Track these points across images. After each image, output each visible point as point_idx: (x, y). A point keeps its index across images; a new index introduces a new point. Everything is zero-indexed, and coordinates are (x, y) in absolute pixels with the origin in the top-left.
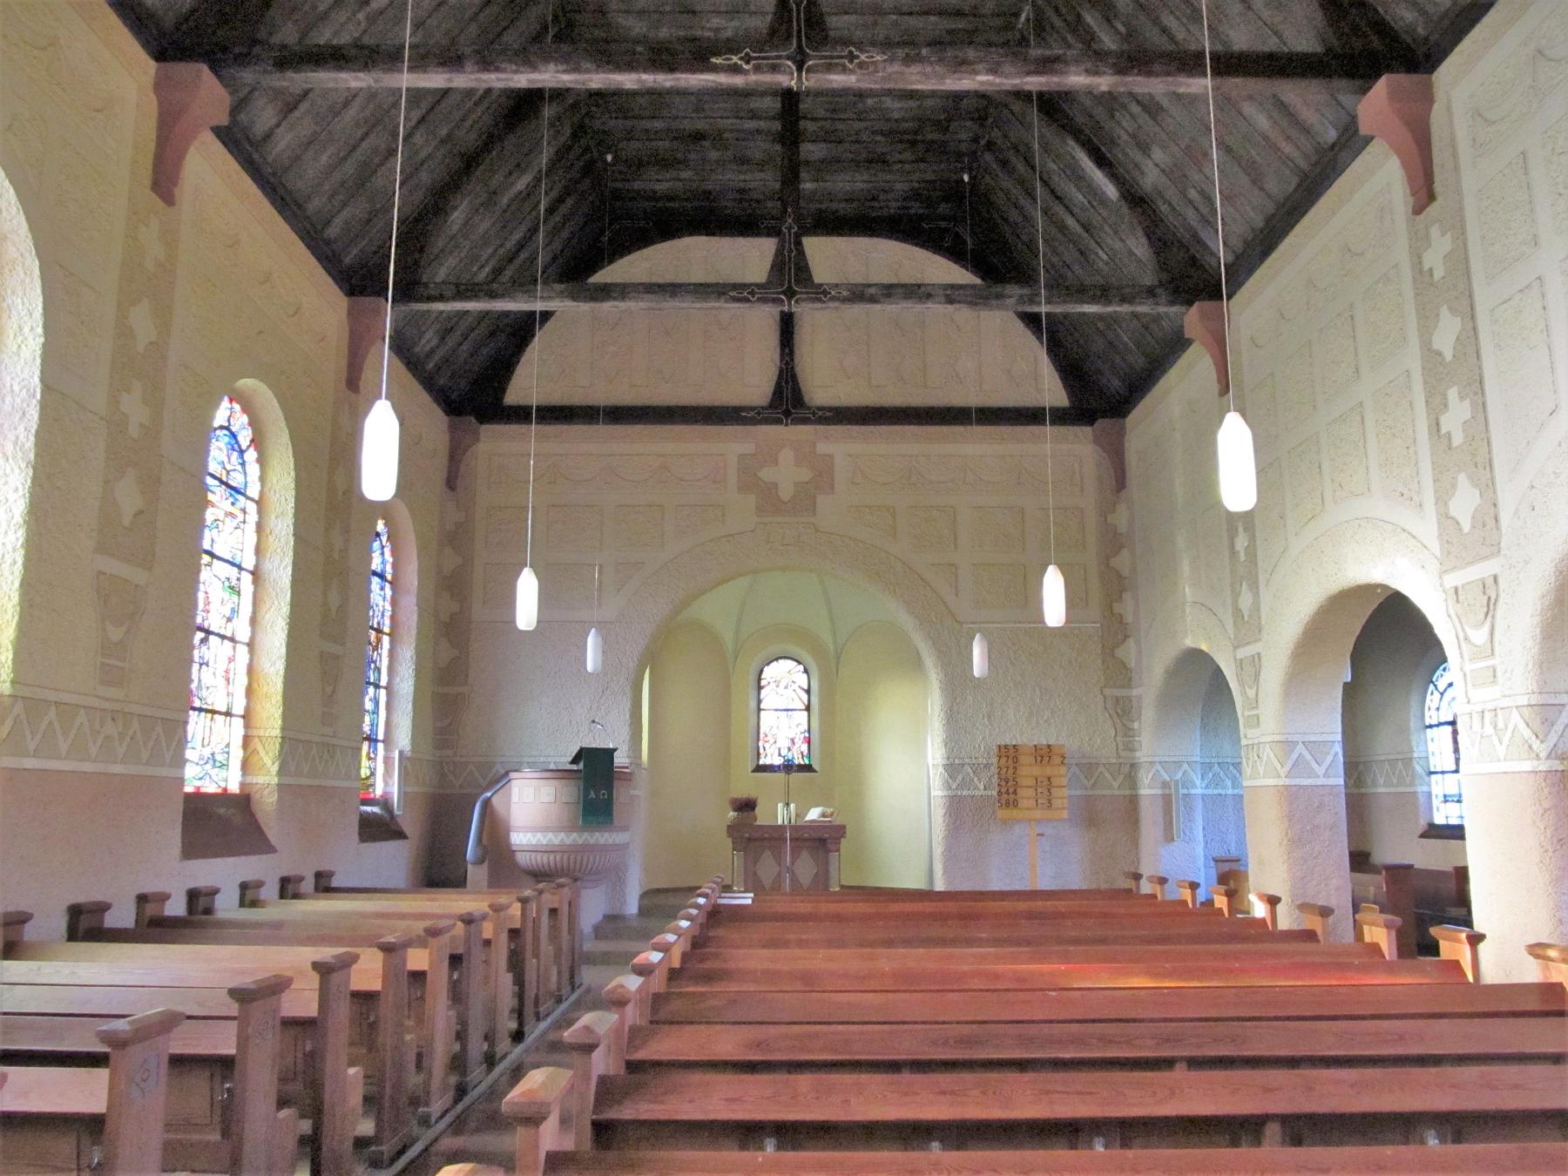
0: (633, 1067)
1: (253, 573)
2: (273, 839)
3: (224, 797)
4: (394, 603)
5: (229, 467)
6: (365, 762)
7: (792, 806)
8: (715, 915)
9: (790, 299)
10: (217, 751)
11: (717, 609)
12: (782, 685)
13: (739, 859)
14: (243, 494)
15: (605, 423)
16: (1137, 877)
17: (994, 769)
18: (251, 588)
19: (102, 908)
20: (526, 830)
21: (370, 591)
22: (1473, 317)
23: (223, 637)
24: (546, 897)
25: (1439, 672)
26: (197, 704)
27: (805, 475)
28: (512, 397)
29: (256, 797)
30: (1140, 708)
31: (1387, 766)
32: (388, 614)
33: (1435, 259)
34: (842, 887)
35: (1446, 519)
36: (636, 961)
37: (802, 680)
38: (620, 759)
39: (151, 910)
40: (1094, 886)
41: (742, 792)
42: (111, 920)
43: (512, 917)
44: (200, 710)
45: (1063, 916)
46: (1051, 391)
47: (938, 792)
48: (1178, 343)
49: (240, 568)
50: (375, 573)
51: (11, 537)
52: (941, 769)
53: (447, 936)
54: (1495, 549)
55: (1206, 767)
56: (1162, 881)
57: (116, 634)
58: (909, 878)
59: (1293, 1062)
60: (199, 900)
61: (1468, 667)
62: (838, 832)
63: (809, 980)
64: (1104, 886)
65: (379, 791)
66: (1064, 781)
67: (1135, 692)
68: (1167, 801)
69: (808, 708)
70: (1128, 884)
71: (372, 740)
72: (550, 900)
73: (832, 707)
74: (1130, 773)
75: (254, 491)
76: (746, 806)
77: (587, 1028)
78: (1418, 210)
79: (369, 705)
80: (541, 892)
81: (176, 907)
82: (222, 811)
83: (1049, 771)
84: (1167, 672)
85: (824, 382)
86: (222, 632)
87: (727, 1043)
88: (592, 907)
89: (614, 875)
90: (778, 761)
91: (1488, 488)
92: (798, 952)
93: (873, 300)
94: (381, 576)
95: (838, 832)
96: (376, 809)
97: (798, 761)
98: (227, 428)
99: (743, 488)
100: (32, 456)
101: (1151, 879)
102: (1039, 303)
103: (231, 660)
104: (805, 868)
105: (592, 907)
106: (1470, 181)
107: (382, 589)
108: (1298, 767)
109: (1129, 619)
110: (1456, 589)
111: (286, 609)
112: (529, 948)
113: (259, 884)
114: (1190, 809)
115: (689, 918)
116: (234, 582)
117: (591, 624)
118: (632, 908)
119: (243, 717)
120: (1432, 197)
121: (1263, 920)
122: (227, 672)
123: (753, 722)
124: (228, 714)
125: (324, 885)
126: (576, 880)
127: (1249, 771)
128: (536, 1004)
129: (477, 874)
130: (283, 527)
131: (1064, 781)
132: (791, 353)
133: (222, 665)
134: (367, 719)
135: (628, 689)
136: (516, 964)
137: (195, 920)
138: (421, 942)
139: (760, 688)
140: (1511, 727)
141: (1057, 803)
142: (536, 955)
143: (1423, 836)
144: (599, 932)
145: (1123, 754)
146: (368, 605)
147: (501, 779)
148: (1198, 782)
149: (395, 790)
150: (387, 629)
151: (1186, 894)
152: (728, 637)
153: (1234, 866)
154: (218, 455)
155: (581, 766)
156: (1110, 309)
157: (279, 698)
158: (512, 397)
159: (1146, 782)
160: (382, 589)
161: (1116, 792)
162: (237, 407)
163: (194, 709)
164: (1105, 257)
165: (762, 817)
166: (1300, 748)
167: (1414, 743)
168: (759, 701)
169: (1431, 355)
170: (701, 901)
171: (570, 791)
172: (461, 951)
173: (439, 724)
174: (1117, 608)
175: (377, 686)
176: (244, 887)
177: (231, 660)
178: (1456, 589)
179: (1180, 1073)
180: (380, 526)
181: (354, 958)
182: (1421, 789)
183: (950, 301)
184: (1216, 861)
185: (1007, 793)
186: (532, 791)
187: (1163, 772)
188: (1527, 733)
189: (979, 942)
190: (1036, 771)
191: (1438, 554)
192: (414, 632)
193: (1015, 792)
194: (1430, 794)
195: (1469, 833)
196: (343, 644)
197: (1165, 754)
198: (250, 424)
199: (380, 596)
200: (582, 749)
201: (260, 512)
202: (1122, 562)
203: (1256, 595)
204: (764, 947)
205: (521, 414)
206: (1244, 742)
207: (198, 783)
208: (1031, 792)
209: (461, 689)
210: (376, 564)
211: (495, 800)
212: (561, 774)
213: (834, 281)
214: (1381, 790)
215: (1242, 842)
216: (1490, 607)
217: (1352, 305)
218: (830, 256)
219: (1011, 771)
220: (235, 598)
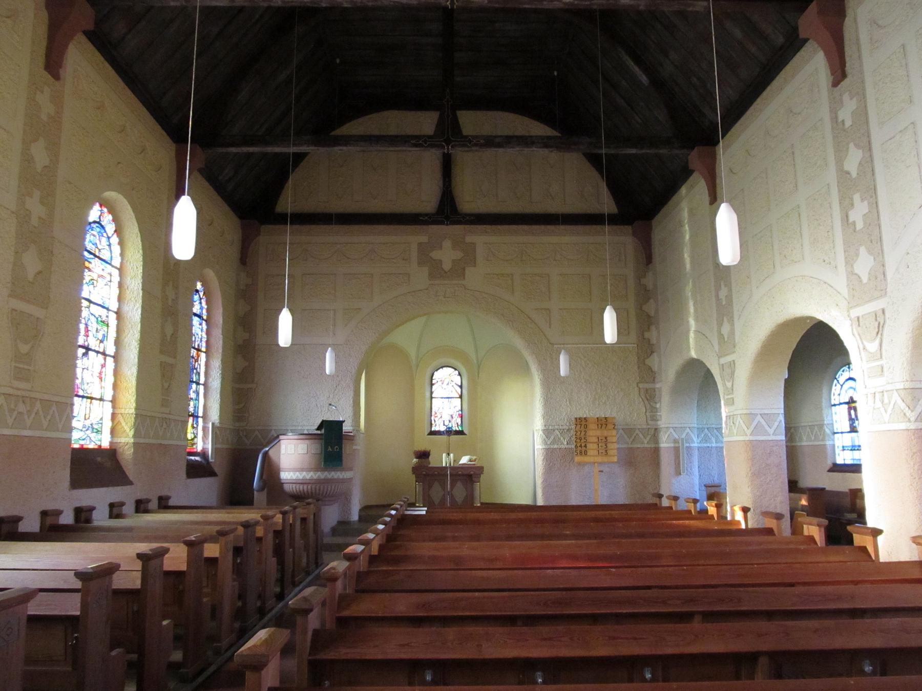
0: (343, 622)
1: (116, 313)
2: (131, 477)
3: (99, 450)
4: (208, 333)
6: (190, 430)
7: (452, 455)
8: (403, 521)
9: (448, 145)
10: (94, 422)
11: (406, 336)
12: (446, 383)
13: (419, 487)
14: (110, 264)
15: (336, 224)
16: (660, 496)
17: (573, 433)
18: (115, 322)
19: (17, 520)
20: (289, 470)
21: (192, 326)
22: (870, 149)
23: (98, 352)
24: (300, 511)
25: (840, 372)
26: (81, 393)
28: (279, 209)
29: (120, 451)
30: (661, 395)
31: (808, 429)
32: (204, 340)
33: (846, 115)
34: (482, 504)
35: (852, 275)
36: (346, 551)
37: (458, 380)
38: (347, 427)
39: (49, 521)
40: (632, 502)
41: (421, 447)
42: (23, 527)
43: (276, 523)
44: (83, 397)
45: (616, 520)
46: (607, 204)
47: (539, 446)
48: (685, 173)
49: (108, 309)
50: (195, 315)
52: (541, 432)
53: (232, 535)
54: (883, 293)
55: (700, 430)
56: (676, 498)
57: (24, 348)
58: (521, 497)
59: (770, 615)
60: (83, 515)
62: (480, 469)
63: (458, 563)
64: (640, 502)
65: (199, 448)
67: (658, 386)
68: (677, 450)
69: (461, 397)
70: (655, 500)
71: (195, 416)
72: (300, 511)
73: (475, 396)
75: (117, 262)
76: (423, 455)
77: (305, 599)
78: (835, 84)
79: (193, 395)
80: (295, 508)
81: (67, 518)
82: (99, 459)
83: (605, 433)
85: (470, 199)
86: (97, 349)
87: (402, 605)
88: (330, 516)
89: (344, 498)
90: (443, 429)
91: (879, 254)
92: (452, 544)
93: (499, 145)
94: (199, 316)
95: (480, 469)
96: (197, 458)
97: (455, 428)
98: (98, 223)
99: (421, 263)
101: (669, 497)
102: (601, 148)
103: (103, 366)
104: (459, 492)
105: (330, 516)
107: (201, 324)
108: (758, 429)
109: (654, 341)
110: (858, 318)
112: (287, 543)
113: (122, 504)
114: (690, 455)
115: (385, 523)
116: (104, 318)
117: (329, 345)
118: (355, 517)
119: (111, 401)
120: (844, 75)
122: (100, 373)
123: (428, 405)
124: (101, 399)
125: (164, 504)
126: (318, 500)
128: (293, 576)
129: (259, 497)
130: (135, 284)
131: (615, 439)
132: (450, 181)
133: (98, 368)
134: (192, 403)
136: (279, 551)
137: (81, 526)
138: (212, 539)
139: (432, 385)
140: (892, 403)
141: (610, 452)
142: (292, 546)
143: (830, 471)
144: (334, 531)
145: (650, 422)
146: (191, 334)
147: (274, 439)
148: (695, 439)
149: (209, 447)
150: (204, 349)
151: (691, 506)
152: (413, 353)
154: (91, 239)
155: (323, 431)
156: (644, 151)
157: (134, 389)
158: (279, 209)
159: (664, 439)
160: (201, 324)
161: (646, 446)
162: (105, 210)
163: (79, 396)
164: (639, 121)
165: (433, 462)
168: (432, 393)
169: (843, 174)
170: (393, 512)
171: (316, 447)
172: (241, 544)
173: (237, 407)
174: (646, 335)
175: (198, 384)
176: (112, 506)
177: (103, 366)
178: (858, 318)
179: (697, 624)
180: (199, 286)
181: (167, 550)
182: (828, 443)
183: (546, 146)
184: (706, 486)
185: (581, 446)
186: (293, 446)
187: (674, 433)
188: (903, 406)
189: (566, 537)
190: (598, 433)
191: (846, 297)
192: (221, 351)
193: (585, 446)
194: (834, 446)
195: (864, 469)
196: (175, 358)
197: (676, 423)
198: (113, 220)
199: (198, 329)
200: (323, 422)
201: (121, 275)
202: (650, 308)
203: (732, 325)
204: (431, 541)
205: (281, 219)
207: (82, 442)
208: (595, 446)
209: (250, 386)
210: (196, 309)
211: (271, 453)
212: (310, 436)
213: (474, 134)
214: (804, 444)
215: (722, 473)
216: (880, 329)
218: (472, 122)
219: (583, 433)
220: (105, 328)
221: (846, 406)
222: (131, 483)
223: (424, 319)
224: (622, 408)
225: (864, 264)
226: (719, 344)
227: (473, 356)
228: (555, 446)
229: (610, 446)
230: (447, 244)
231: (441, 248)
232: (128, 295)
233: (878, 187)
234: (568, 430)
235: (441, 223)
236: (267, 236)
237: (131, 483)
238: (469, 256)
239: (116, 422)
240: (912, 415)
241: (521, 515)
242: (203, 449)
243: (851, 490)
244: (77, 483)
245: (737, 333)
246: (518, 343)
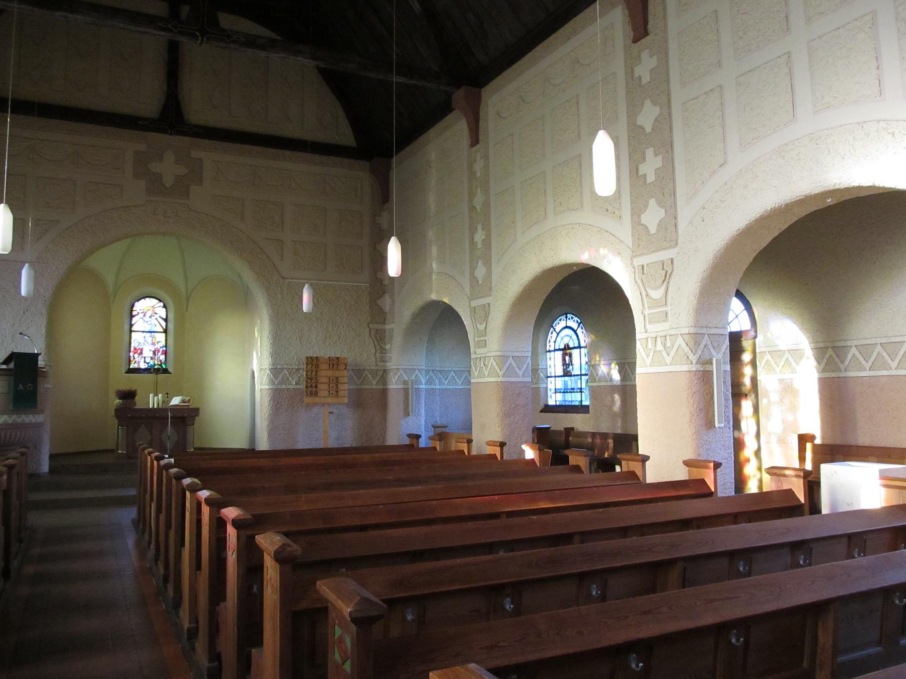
11: (104, 262)
13: (122, 431)
27: (182, 170)
34: (195, 449)
35: (638, 225)
37: (162, 312)
38: (41, 363)
41: (125, 387)
46: (345, 136)
48: (443, 109)
52: (268, 372)
61: (647, 312)
62: (195, 412)
66: (346, 380)
67: (388, 327)
69: (165, 331)
73: (179, 328)
74: (383, 375)
76: (128, 396)
83: (337, 374)
84: (413, 314)
85: (198, 111)
90: (143, 366)
95: (195, 412)
106: (673, 26)
108: (509, 371)
110: (643, 267)
118: (45, 468)
121: (533, 460)
123: (127, 338)
127: (476, 374)
135: (44, 311)
139: (132, 316)
141: (341, 393)
152: (110, 279)
153: (444, 430)
155: (12, 365)
156: (412, 82)
159: (394, 381)
161: (374, 387)
165: (139, 403)
166: (510, 360)
167: (540, 361)
168: (131, 325)
178: (643, 267)
185: (311, 386)
188: (687, 349)
190: (330, 373)
193: (316, 387)
206: (473, 356)
217: (577, 96)
219: (314, 373)
221: (560, 353)
223: (124, 243)
224: (352, 348)
225: (653, 216)
226: (471, 286)
229: (341, 387)
230: (170, 156)
233: (675, 144)
234: (297, 370)
240: (694, 358)
241: (309, 460)
243: (565, 429)
245: (494, 278)
246: (248, 276)
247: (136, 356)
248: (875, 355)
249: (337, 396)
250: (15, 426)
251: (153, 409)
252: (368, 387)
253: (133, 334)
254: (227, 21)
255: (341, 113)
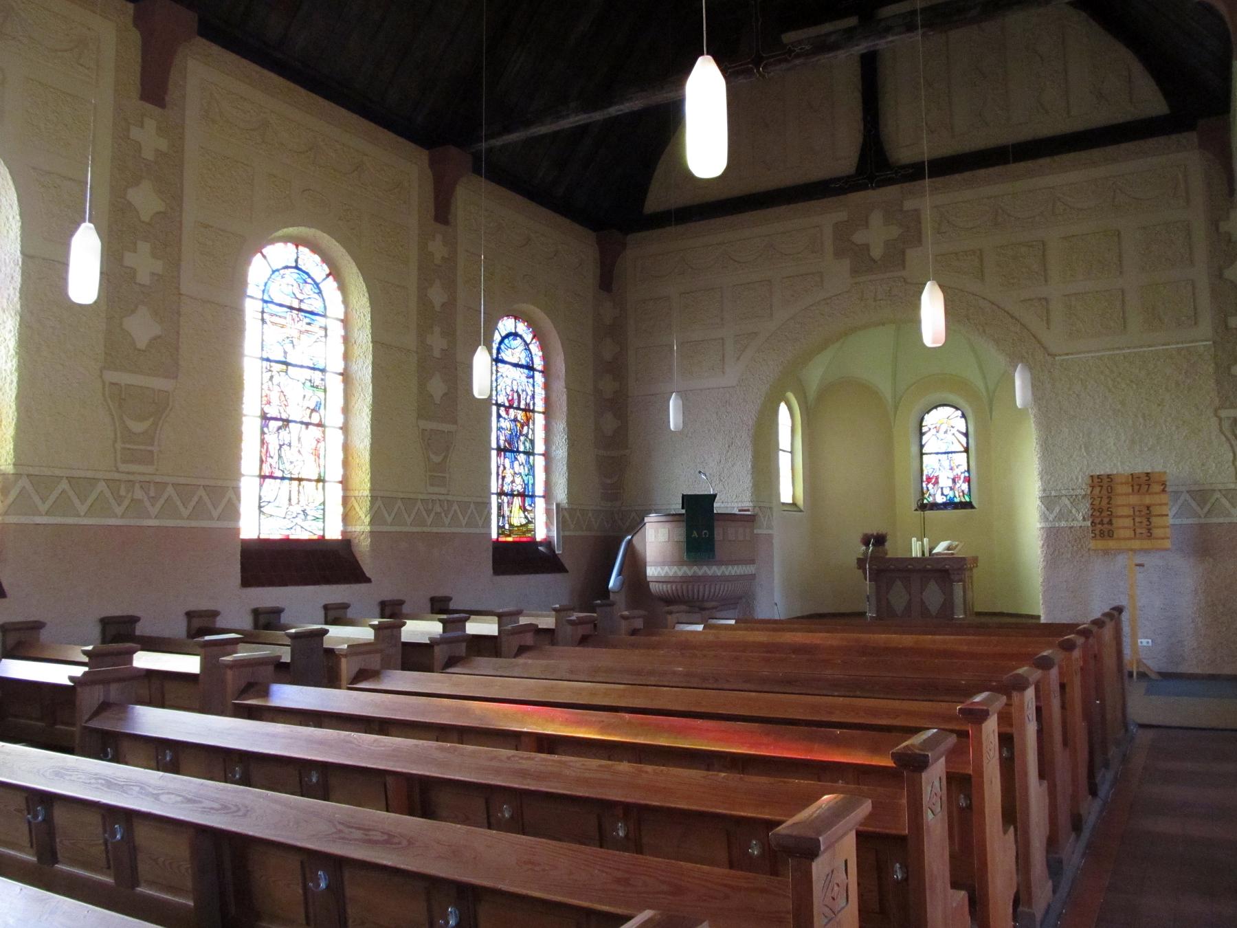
2: (368, 570)
5: (301, 297)
12: (942, 431)
13: (867, 586)
27: (895, 231)
37: (961, 425)
51: (9, 364)
65: (540, 535)
69: (967, 450)
83: (1148, 500)
90: (940, 499)
99: (839, 254)
100: (18, 306)
111: (369, 399)
135: (748, 443)
139: (922, 434)
141: (1157, 532)
147: (637, 525)
150: (540, 406)
152: (886, 389)
168: (922, 446)
171: (680, 532)
190: (1134, 500)
192: (565, 409)
193: (1110, 523)
196: (455, 422)
211: (635, 541)
212: (673, 518)
219: (1105, 502)
222: (368, 580)
227: (980, 384)
228: (1063, 524)
230: (876, 218)
231: (867, 225)
232: (357, 351)
235: (863, 187)
236: (642, 250)
237: (368, 580)
238: (912, 234)
239: (349, 506)
242: (548, 537)
244: (249, 579)
247: (930, 486)
248: (196, 499)
249: (1150, 535)
250: (695, 579)
251: (916, 558)
252: (1221, 520)
253: (925, 457)
254: (789, 37)
255: (1137, 68)
